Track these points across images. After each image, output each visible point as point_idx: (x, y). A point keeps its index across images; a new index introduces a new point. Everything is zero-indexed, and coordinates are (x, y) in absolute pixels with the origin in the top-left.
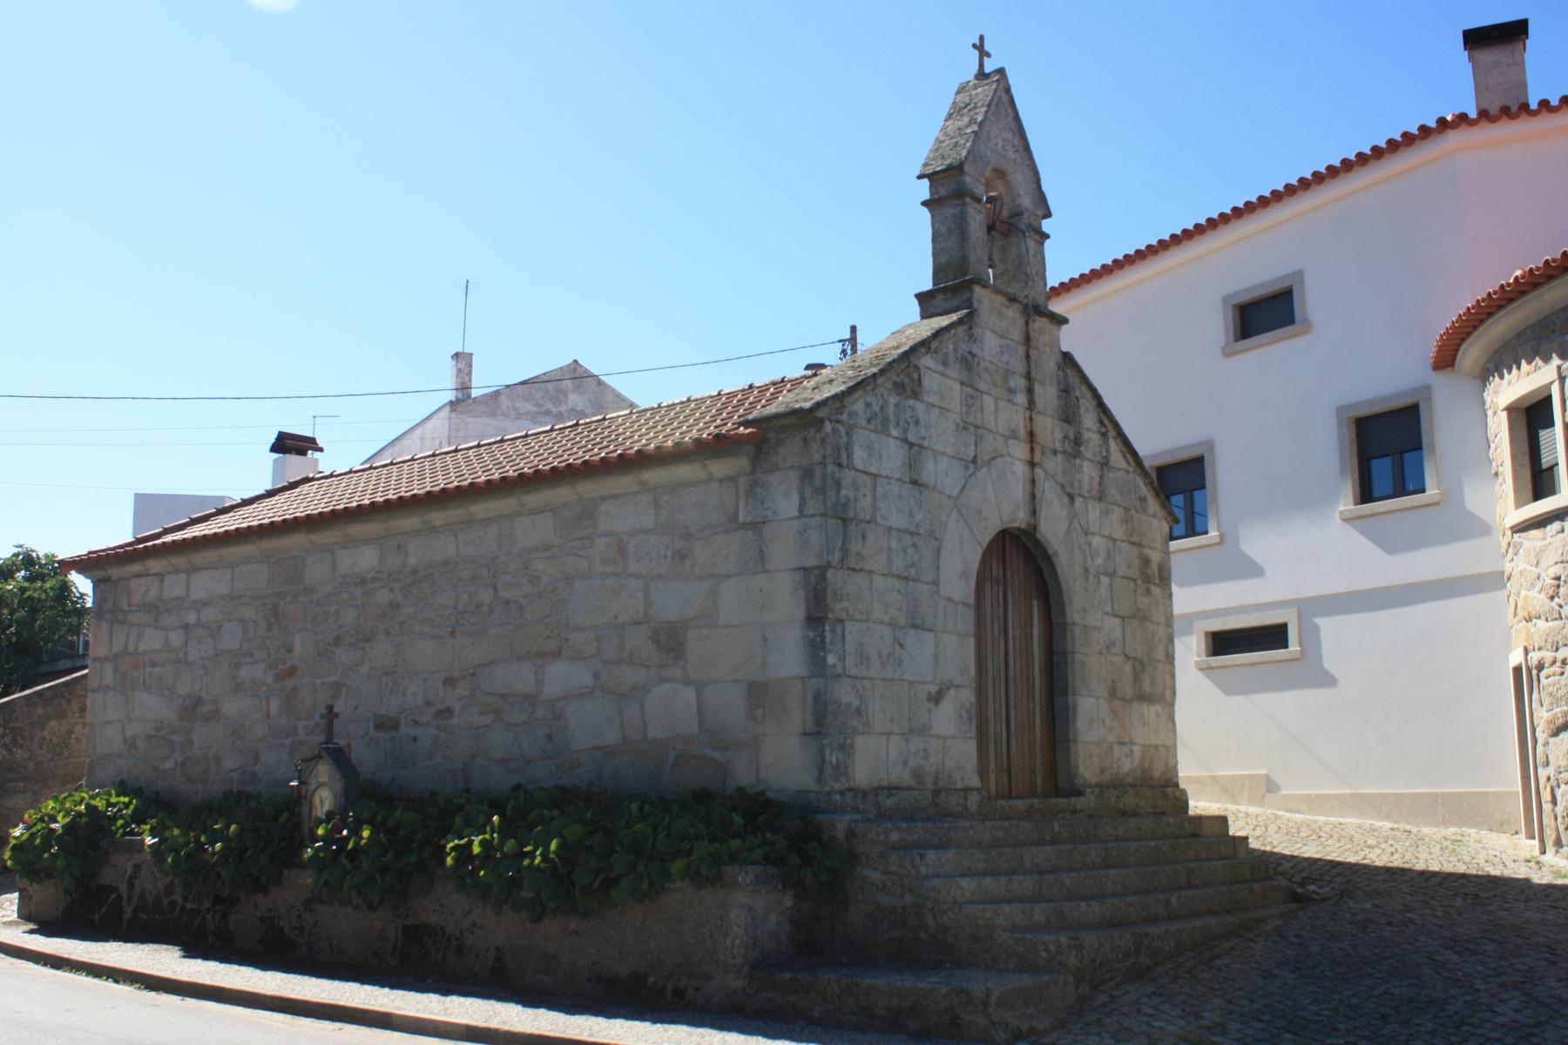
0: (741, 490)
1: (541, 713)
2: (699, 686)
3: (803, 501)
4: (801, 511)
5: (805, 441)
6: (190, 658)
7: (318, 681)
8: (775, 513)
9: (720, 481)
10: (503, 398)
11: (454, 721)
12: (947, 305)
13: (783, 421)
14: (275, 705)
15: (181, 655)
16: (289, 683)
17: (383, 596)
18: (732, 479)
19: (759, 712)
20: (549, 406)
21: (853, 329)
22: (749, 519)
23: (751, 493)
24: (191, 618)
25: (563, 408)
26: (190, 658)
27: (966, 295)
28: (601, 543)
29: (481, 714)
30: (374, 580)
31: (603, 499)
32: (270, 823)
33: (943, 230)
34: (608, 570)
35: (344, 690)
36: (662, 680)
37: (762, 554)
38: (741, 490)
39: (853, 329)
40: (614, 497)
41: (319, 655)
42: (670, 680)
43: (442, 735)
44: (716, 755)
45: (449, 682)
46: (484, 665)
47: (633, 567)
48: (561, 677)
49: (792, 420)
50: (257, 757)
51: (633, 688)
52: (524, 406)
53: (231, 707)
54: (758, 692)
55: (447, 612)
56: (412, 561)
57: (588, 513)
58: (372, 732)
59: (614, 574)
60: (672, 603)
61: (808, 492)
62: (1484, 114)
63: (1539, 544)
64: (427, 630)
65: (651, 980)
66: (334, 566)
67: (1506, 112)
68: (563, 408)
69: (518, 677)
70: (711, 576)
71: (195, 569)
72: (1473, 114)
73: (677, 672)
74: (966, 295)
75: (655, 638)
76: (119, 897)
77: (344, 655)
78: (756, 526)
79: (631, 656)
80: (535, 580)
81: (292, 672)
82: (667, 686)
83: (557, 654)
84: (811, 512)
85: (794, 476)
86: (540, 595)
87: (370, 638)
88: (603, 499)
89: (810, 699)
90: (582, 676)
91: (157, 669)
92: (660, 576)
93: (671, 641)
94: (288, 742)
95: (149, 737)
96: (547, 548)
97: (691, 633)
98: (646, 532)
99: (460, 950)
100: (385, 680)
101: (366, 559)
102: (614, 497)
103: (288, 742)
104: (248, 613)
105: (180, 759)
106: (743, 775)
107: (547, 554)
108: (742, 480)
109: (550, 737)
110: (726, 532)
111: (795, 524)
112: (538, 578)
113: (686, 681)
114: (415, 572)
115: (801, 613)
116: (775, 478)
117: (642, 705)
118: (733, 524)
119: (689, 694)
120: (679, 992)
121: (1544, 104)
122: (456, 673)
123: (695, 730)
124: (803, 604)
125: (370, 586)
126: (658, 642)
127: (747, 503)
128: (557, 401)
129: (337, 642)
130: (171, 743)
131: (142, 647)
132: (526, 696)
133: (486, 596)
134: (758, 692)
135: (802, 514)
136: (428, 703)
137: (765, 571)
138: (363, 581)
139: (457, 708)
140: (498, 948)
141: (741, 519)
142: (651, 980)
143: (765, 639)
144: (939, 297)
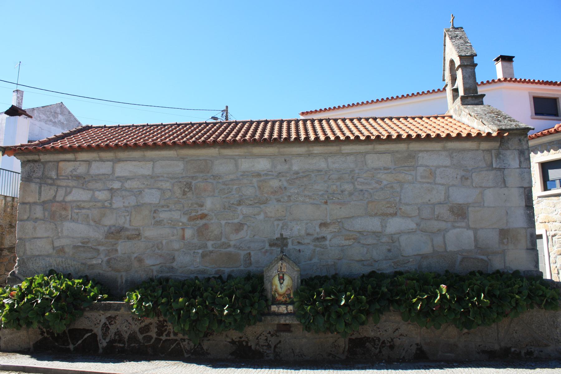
0: (493, 155)
1: (384, 240)
2: (475, 230)
3: (520, 162)
4: (520, 166)
5: (520, 140)
6: (114, 206)
7: (223, 222)
8: (509, 165)
9: (483, 151)
10: (35, 111)
11: (327, 243)
12: (473, 102)
13: (515, 131)
14: (189, 233)
15: (106, 204)
16: (201, 222)
17: (275, 183)
18: (489, 151)
19: (505, 241)
20: (52, 118)
21: (227, 107)
22: (498, 167)
23: (498, 155)
24: (116, 185)
25: (56, 120)
26: (114, 206)
27: (481, 100)
28: (421, 169)
29: (346, 240)
30: (266, 175)
31: (421, 151)
32: (249, 290)
33: (467, 76)
34: (424, 180)
35: (245, 227)
36: (454, 227)
37: (504, 181)
38: (493, 155)
39: (227, 107)
40: (427, 151)
41: (224, 209)
42: (459, 227)
43: (318, 249)
44: (484, 258)
45: (323, 225)
46: (347, 218)
47: (438, 180)
48: (395, 225)
49: (518, 132)
50: (174, 258)
51: (439, 230)
52: (43, 117)
53: (150, 233)
54: (504, 233)
55: (320, 193)
56: (295, 168)
57: (412, 156)
58: (267, 247)
59: (428, 183)
60: (460, 196)
61: (522, 159)
62: (505, 80)
63: (555, 202)
64: (308, 200)
65: (513, 349)
66: (236, 166)
67: (511, 80)
68: (56, 120)
69: (373, 224)
70: (481, 187)
71: (120, 160)
72: (502, 80)
73: (463, 224)
74: (481, 100)
75: (452, 210)
76: (95, 336)
77: (245, 210)
78: (501, 169)
79: (438, 217)
80: (379, 182)
81: (203, 216)
82: (458, 230)
83: (395, 215)
84: (524, 167)
85: (516, 153)
86: (382, 189)
87: (265, 202)
88: (421, 151)
89: (529, 236)
90: (412, 225)
91: (84, 211)
92: (453, 185)
93: (460, 212)
94: (200, 251)
95: (75, 247)
96: (386, 169)
97: (470, 209)
98: (446, 167)
99: (392, 347)
100: (276, 223)
101: (262, 165)
102: (427, 151)
103: (200, 251)
104: (167, 185)
105: (106, 259)
106: (497, 264)
107: (386, 172)
108: (493, 152)
109: (389, 251)
110: (487, 170)
111: (518, 170)
112: (381, 182)
113: (468, 228)
114: (297, 173)
115: (524, 204)
116: (508, 153)
117: (444, 237)
118: (490, 167)
119: (471, 233)
120: (529, 353)
121: (482, 83)
122: (329, 221)
123: (473, 248)
124: (524, 201)
125: (262, 178)
126: (453, 212)
127: (496, 161)
128: (55, 117)
129: (240, 203)
130: (98, 250)
131: (69, 198)
132: (374, 233)
133: (348, 187)
134: (504, 233)
135: (520, 167)
136: (308, 234)
137: (505, 186)
138: (259, 175)
139: (329, 237)
140: (417, 344)
141: (494, 166)
142: (513, 349)
143: (507, 213)
144: (469, 99)
